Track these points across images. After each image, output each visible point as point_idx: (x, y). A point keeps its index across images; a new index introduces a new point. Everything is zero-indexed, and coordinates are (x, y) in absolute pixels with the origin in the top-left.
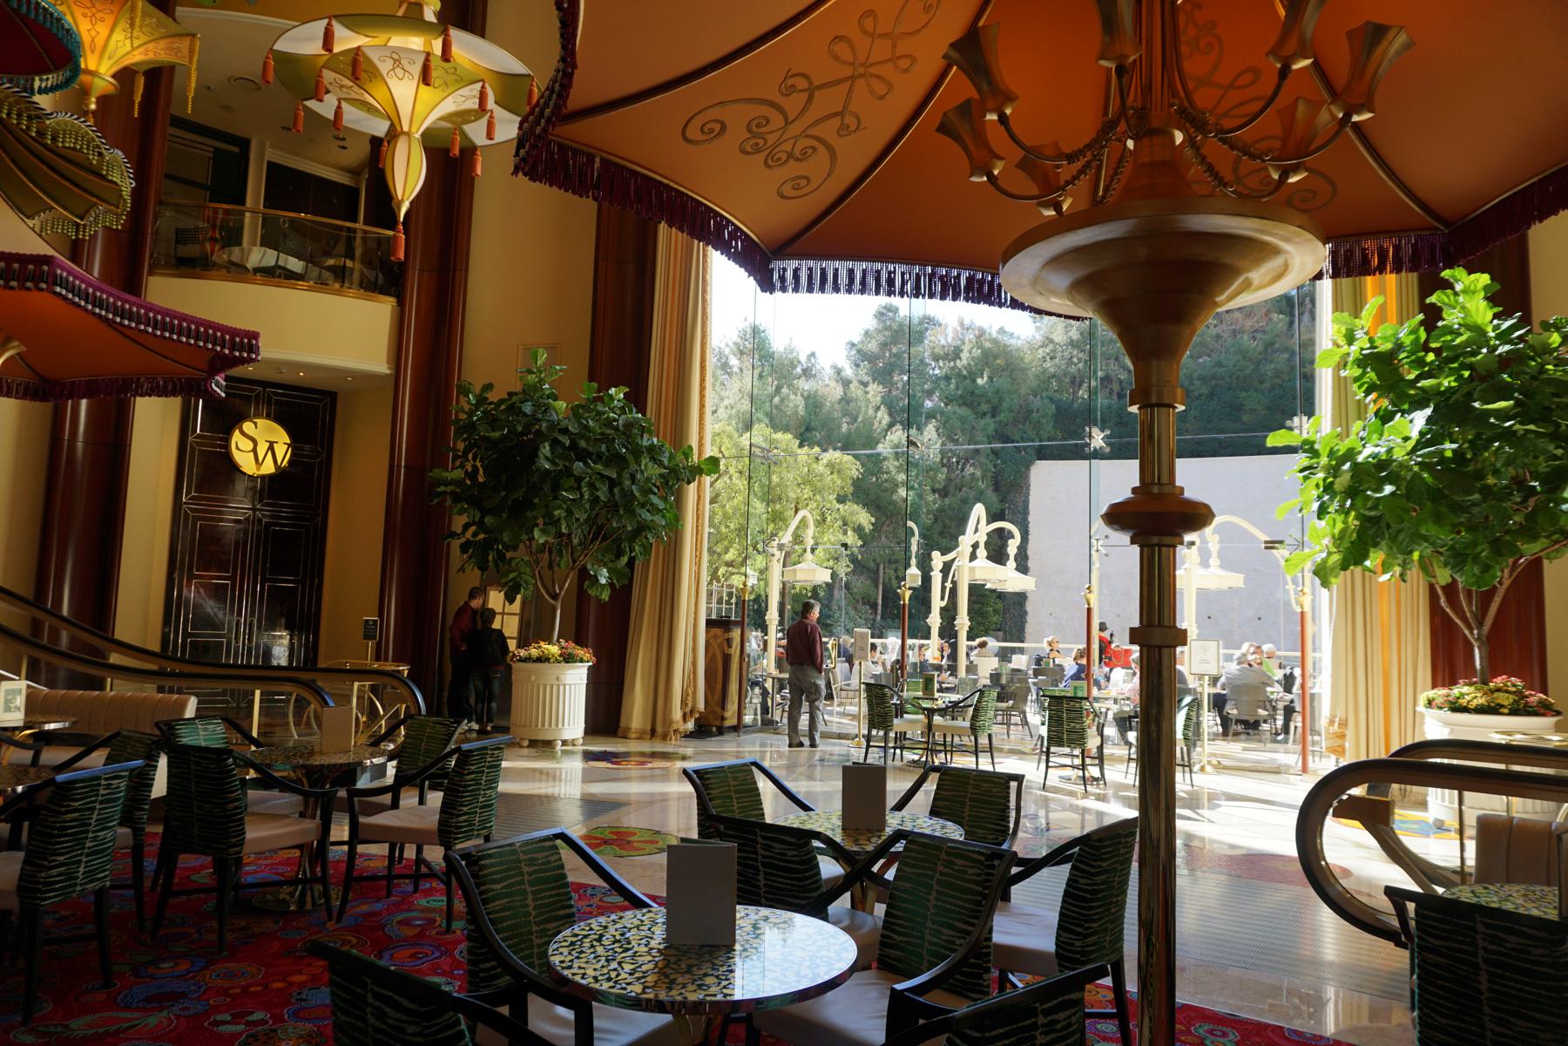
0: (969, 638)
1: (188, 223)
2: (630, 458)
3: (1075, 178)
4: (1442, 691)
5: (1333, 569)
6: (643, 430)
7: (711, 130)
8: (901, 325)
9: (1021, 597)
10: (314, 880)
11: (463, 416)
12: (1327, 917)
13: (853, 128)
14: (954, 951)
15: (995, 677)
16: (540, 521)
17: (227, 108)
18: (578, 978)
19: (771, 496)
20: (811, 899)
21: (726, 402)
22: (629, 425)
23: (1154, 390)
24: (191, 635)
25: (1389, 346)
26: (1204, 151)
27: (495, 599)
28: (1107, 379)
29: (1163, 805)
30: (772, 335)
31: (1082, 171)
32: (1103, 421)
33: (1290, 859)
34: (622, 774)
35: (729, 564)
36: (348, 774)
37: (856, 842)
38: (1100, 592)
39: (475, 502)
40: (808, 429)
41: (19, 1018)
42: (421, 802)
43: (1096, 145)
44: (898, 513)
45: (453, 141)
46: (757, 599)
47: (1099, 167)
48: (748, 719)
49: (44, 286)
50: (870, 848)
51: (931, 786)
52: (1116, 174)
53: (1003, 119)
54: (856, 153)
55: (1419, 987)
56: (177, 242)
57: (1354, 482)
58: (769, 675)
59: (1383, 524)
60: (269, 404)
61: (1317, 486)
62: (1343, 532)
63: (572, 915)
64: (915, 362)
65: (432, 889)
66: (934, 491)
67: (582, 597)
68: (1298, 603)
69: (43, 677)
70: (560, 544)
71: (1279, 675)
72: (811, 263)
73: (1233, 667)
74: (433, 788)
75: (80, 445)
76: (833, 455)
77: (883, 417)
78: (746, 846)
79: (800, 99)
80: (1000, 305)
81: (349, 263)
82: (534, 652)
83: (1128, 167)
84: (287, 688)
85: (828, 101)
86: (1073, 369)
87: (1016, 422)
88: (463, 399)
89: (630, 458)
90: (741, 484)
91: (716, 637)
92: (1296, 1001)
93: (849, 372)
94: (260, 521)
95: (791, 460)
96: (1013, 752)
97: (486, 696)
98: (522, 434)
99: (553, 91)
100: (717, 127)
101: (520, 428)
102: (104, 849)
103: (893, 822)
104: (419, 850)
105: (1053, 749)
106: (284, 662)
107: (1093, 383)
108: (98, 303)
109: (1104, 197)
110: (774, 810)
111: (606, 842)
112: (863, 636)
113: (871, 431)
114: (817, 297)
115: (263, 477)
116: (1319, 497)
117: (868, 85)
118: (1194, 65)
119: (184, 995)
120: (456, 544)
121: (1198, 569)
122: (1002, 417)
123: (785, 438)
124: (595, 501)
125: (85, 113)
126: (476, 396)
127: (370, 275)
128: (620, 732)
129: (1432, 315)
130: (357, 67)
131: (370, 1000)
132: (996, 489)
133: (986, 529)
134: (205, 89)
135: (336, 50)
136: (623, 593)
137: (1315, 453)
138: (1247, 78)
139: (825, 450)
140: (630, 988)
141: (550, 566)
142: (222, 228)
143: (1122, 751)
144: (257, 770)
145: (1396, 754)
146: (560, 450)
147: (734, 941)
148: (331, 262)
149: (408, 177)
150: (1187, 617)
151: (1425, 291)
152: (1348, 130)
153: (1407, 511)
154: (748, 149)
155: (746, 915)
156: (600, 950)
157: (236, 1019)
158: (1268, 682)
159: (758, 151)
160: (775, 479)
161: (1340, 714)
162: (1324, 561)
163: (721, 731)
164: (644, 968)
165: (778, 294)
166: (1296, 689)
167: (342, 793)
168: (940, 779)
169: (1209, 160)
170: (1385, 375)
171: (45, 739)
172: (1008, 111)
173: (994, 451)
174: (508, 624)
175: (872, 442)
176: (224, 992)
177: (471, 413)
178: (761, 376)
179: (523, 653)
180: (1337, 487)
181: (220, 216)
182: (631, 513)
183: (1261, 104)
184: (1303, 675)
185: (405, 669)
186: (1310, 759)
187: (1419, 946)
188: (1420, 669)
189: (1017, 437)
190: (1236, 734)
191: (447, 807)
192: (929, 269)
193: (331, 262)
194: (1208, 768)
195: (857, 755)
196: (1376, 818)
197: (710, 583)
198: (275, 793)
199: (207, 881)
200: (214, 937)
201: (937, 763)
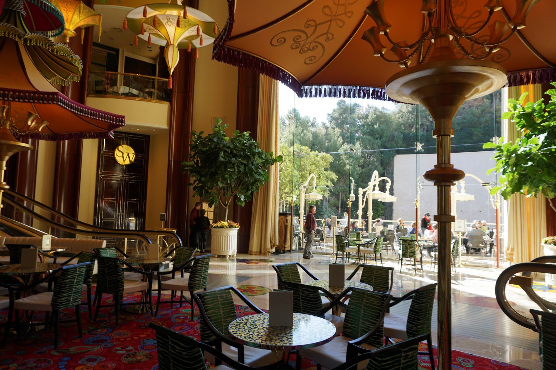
0: (372, 219)
1: (99, 79)
2: (251, 156)
3: (413, 54)
4: (551, 238)
5: (508, 193)
6: (256, 146)
7: (281, 41)
8: (347, 107)
9: (391, 204)
10: (147, 303)
11: (193, 143)
12: (507, 320)
13: (331, 38)
14: (370, 330)
15: (382, 233)
16: (220, 179)
17: (112, 39)
18: (239, 337)
19: (301, 169)
20: (319, 311)
21: (284, 136)
22: (251, 145)
23: (442, 130)
24: (103, 219)
25: (530, 110)
26: (460, 42)
27: (205, 206)
28: (422, 125)
29: (446, 279)
30: (300, 112)
31: (415, 51)
32: (421, 140)
33: (492, 299)
34: (250, 267)
35: (286, 193)
36: (156, 267)
37: (334, 291)
38: (421, 203)
39: (198, 173)
40: (314, 145)
41: (53, 347)
42: (182, 276)
43: (420, 42)
44: (346, 174)
45: (188, 46)
46: (296, 206)
47: (421, 50)
48: (294, 248)
49: (55, 102)
50: (339, 293)
51: (360, 272)
52: (427, 52)
53: (386, 34)
54: (332, 48)
55: (544, 346)
56: (96, 85)
57: (516, 161)
58: (301, 232)
59: (528, 176)
60: (127, 140)
61: (502, 163)
62: (512, 180)
63: (236, 316)
64: (352, 120)
65: (186, 306)
66: (359, 166)
67: (235, 205)
68: (495, 205)
69: (55, 234)
70: (227, 187)
71: (488, 232)
72: (316, 87)
73: (470, 229)
74: (186, 272)
75: (66, 155)
76: (323, 154)
77: (340, 140)
78: (296, 292)
79: (311, 29)
80: (384, 100)
81: (153, 90)
82: (219, 224)
83: (432, 49)
84: (135, 237)
85: (322, 29)
86: (410, 121)
87: (388, 141)
88: (193, 137)
89: (251, 156)
90: (290, 165)
91: (282, 219)
92: (495, 350)
93: (328, 124)
94: (125, 180)
95: (308, 156)
96: (389, 259)
97: (202, 240)
98: (214, 149)
99: (226, 30)
100: (283, 40)
101: (213, 147)
102: (78, 293)
103: (347, 284)
104: (182, 293)
105: (404, 258)
106: (134, 229)
107: (417, 126)
108: (72, 107)
109: (422, 62)
110: (305, 280)
111: (245, 291)
112: (335, 218)
113: (336, 145)
114: (318, 98)
115: (126, 165)
116: (503, 167)
117: (336, 22)
118: (456, 10)
119: (105, 341)
120: (191, 187)
121: (458, 193)
122: (384, 139)
123: (306, 148)
124: (239, 172)
125: (65, 43)
126: (197, 136)
127: (160, 94)
128: (249, 252)
129: (547, 99)
130: (155, 22)
131: (170, 343)
132: (382, 165)
133: (378, 179)
134: (104, 32)
135: (148, 16)
136: (249, 204)
137: (501, 151)
138: (477, 14)
139: (320, 152)
140: (257, 341)
141: (224, 195)
142: (110, 80)
143: (429, 260)
144: (127, 264)
145: (533, 261)
146: (227, 154)
147: (292, 325)
148: (147, 90)
149: (173, 60)
150: (454, 212)
151: (544, 89)
152: (516, 33)
153: (537, 171)
154: (294, 47)
155: (297, 316)
156: (246, 328)
157: (123, 349)
158: (484, 234)
159: (297, 48)
160: (302, 163)
161: (511, 246)
162: (505, 190)
163: (284, 252)
164: (262, 334)
165: (304, 98)
166: (494, 237)
167: (156, 273)
168: (364, 269)
169: (462, 45)
170: (529, 121)
171: (57, 254)
172: (388, 31)
173: (381, 152)
174: (210, 215)
175: (336, 149)
176: (118, 340)
177: (196, 142)
178: (296, 126)
179: (215, 225)
180: (510, 163)
181: (110, 76)
182: (252, 176)
183: (482, 24)
184: (497, 232)
185: (175, 231)
186: (500, 262)
187: (543, 331)
188: (542, 232)
189: (389, 146)
190: (472, 253)
191: (191, 279)
192: (358, 88)
193: (147, 90)
194: (461, 266)
195: (333, 260)
196: (526, 284)
197: (280, 200)
198: (133, 273)
199: (111, 302)
200: (114, 321)
201: (361, 263)
